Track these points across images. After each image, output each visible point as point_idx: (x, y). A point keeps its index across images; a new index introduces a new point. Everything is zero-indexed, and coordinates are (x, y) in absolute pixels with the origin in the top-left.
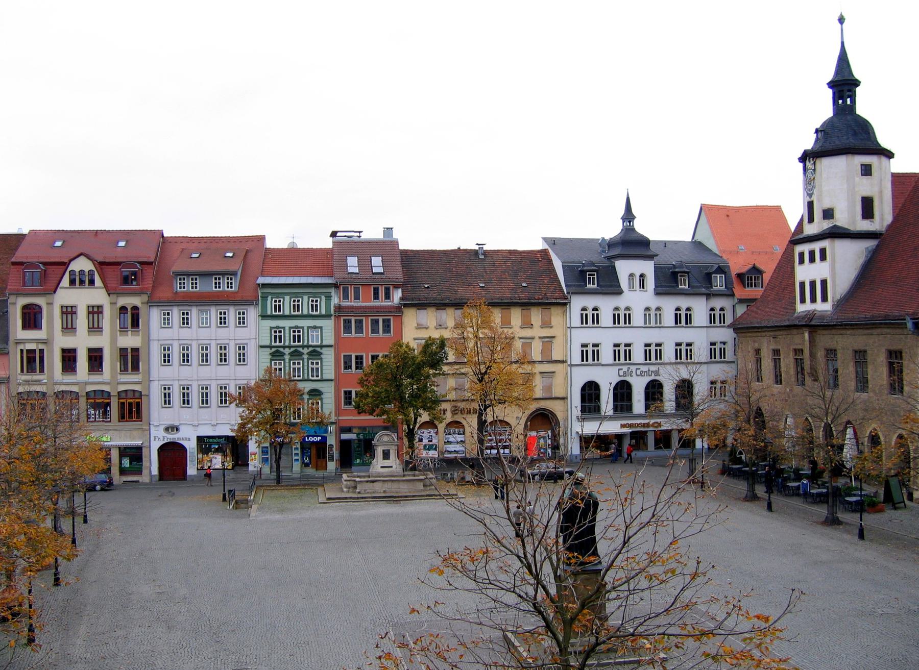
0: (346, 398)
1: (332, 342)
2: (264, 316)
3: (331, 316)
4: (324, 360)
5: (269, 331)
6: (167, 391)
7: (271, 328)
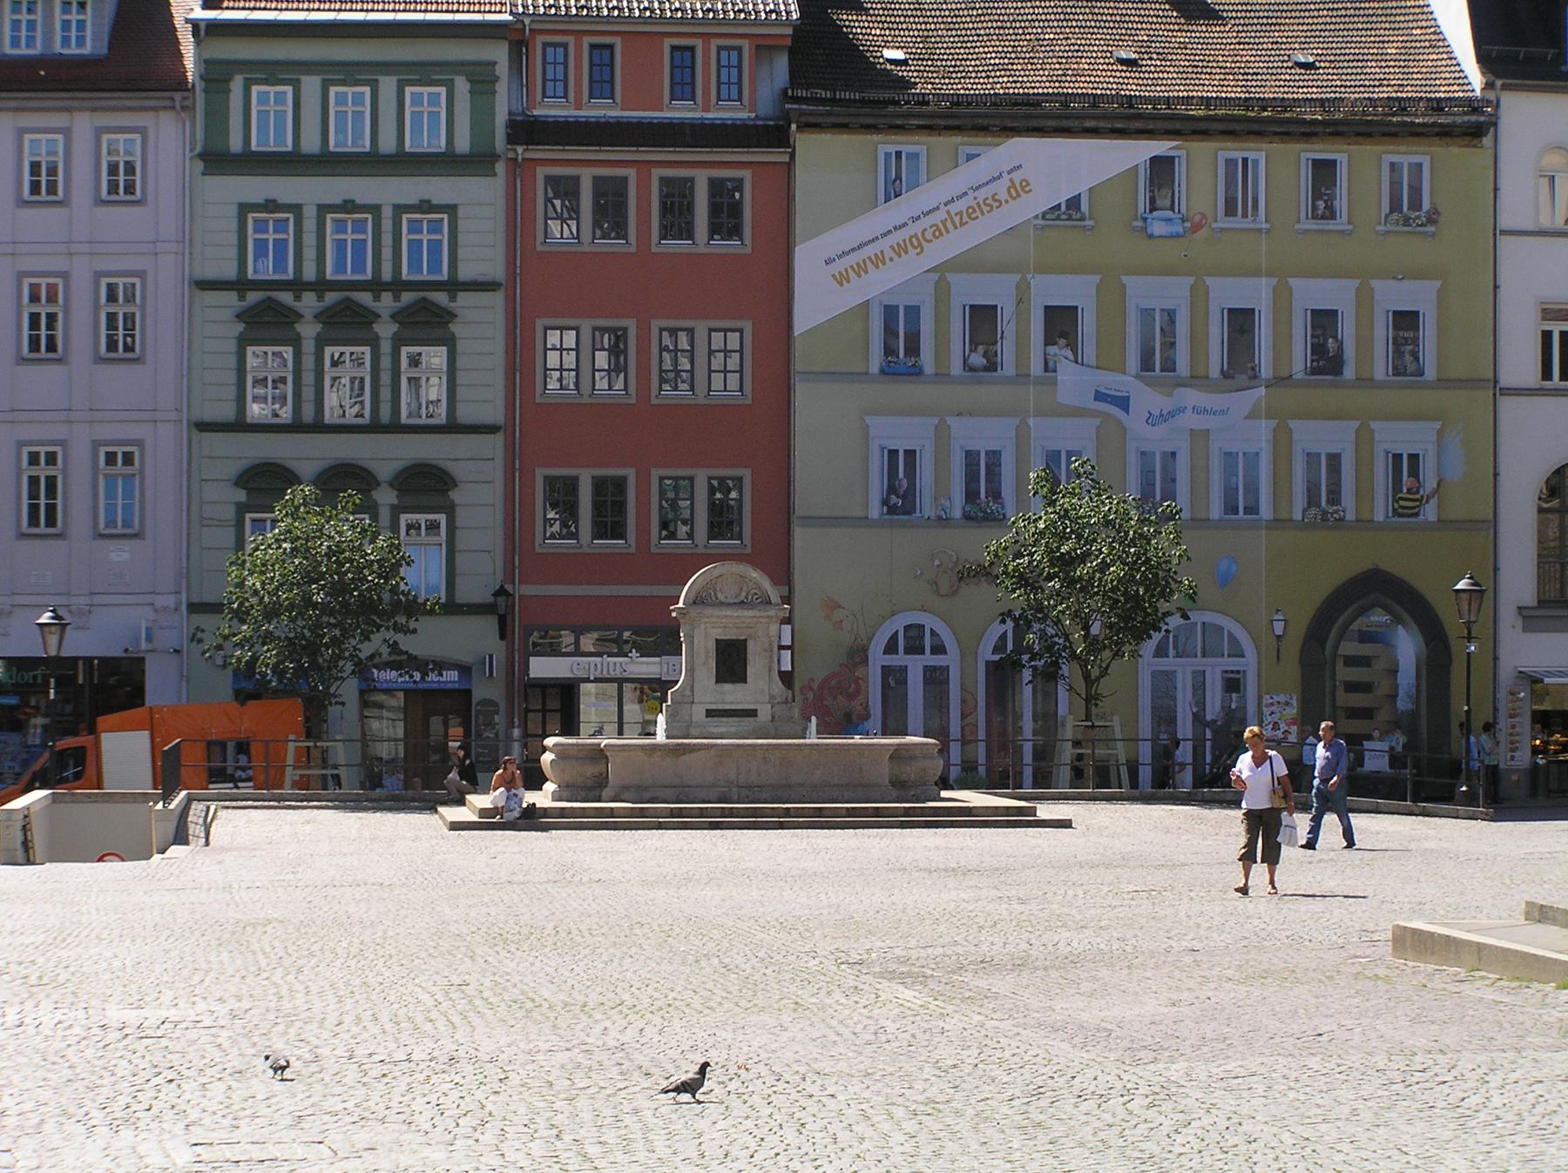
0: (620, 507)
1: (494, 268)
2: (217, 160)
3: (495, 157)
4: (461, 346)
5: (234, 225)
6: (43, 471)
7: (244, 209)
